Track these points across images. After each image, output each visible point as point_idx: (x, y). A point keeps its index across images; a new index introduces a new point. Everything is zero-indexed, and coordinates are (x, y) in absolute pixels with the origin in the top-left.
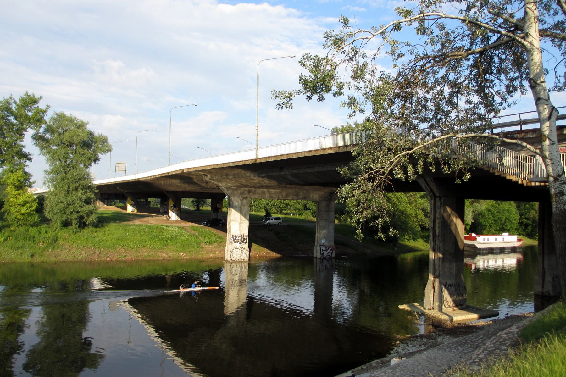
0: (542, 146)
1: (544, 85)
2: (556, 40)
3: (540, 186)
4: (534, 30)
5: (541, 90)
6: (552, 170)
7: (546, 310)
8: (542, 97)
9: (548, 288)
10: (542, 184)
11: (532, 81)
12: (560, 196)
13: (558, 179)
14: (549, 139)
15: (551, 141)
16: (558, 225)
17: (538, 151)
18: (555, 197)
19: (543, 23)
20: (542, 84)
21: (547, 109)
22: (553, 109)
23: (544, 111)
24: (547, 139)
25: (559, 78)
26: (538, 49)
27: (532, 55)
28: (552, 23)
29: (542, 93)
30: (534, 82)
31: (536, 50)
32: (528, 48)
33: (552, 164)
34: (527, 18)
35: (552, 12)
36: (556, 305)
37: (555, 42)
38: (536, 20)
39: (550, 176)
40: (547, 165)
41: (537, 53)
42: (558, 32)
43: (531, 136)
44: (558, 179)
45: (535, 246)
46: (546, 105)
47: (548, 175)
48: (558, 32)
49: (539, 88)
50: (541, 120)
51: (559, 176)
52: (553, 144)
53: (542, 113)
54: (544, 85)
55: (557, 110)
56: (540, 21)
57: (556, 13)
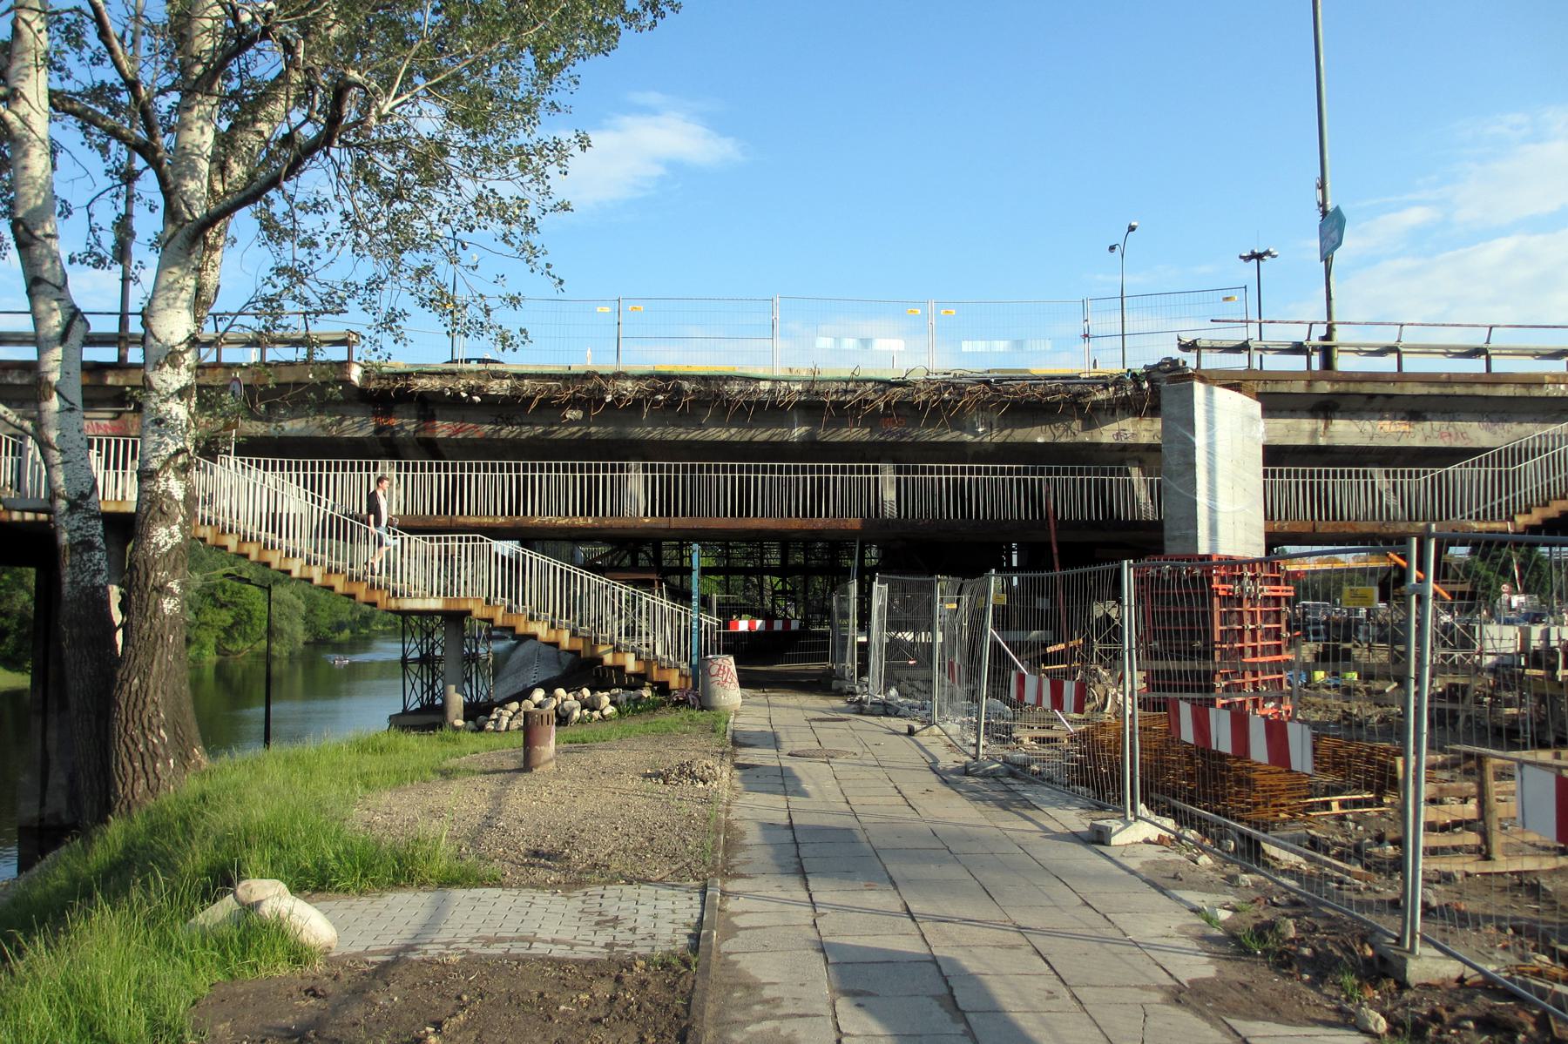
0: (40, 412)
1: (55, 245)
2: (95, 130)
3: (35, 523)
4: (35, 86)
5: (46, 257)
6: (65, 480)
7: (36, 869)
8: (46, 276)
9: (58, 802)
10: (43, 517)
11: (21, 228)
12: (84, 550)
13: (81, 506)
14: (60, 394)
15: (66, 400)
16: (75, 631)
17: (27, 424)
18: (71, 555)
19: (63, 74)
20: (48, 241)
21: (59, 312)
22: (75, 315)
23: (51, 317)
24: (55, 394)
25: (98, 233)
26: (43, 142)
27: (26, 155)
28: (88, 82)
29: (48, 265)
30: (27, 230)
31: (38, 143)
32: (17, 132)
33: (64, 463)
34: (18, 48)
35: (87, 53)
36: (63, 849)
37: (92, 135)
38: (40, 62)
39: (59, 496)
40: (53, 466)
41: (40, 152)
42: (103, 111)
43: (18, 382)
44: (81, 506)
45: (26, 690)
46: (57, 300)
47: (53, 495)
48: (103, 111)
49: (38, 251)
50: (42, 338)
51: (84, 496)
52: (71, 410)
53: (45, 320)
54: (55, 245)
55: (85, 320)
56: (51, 64)
57: (98, 59)
